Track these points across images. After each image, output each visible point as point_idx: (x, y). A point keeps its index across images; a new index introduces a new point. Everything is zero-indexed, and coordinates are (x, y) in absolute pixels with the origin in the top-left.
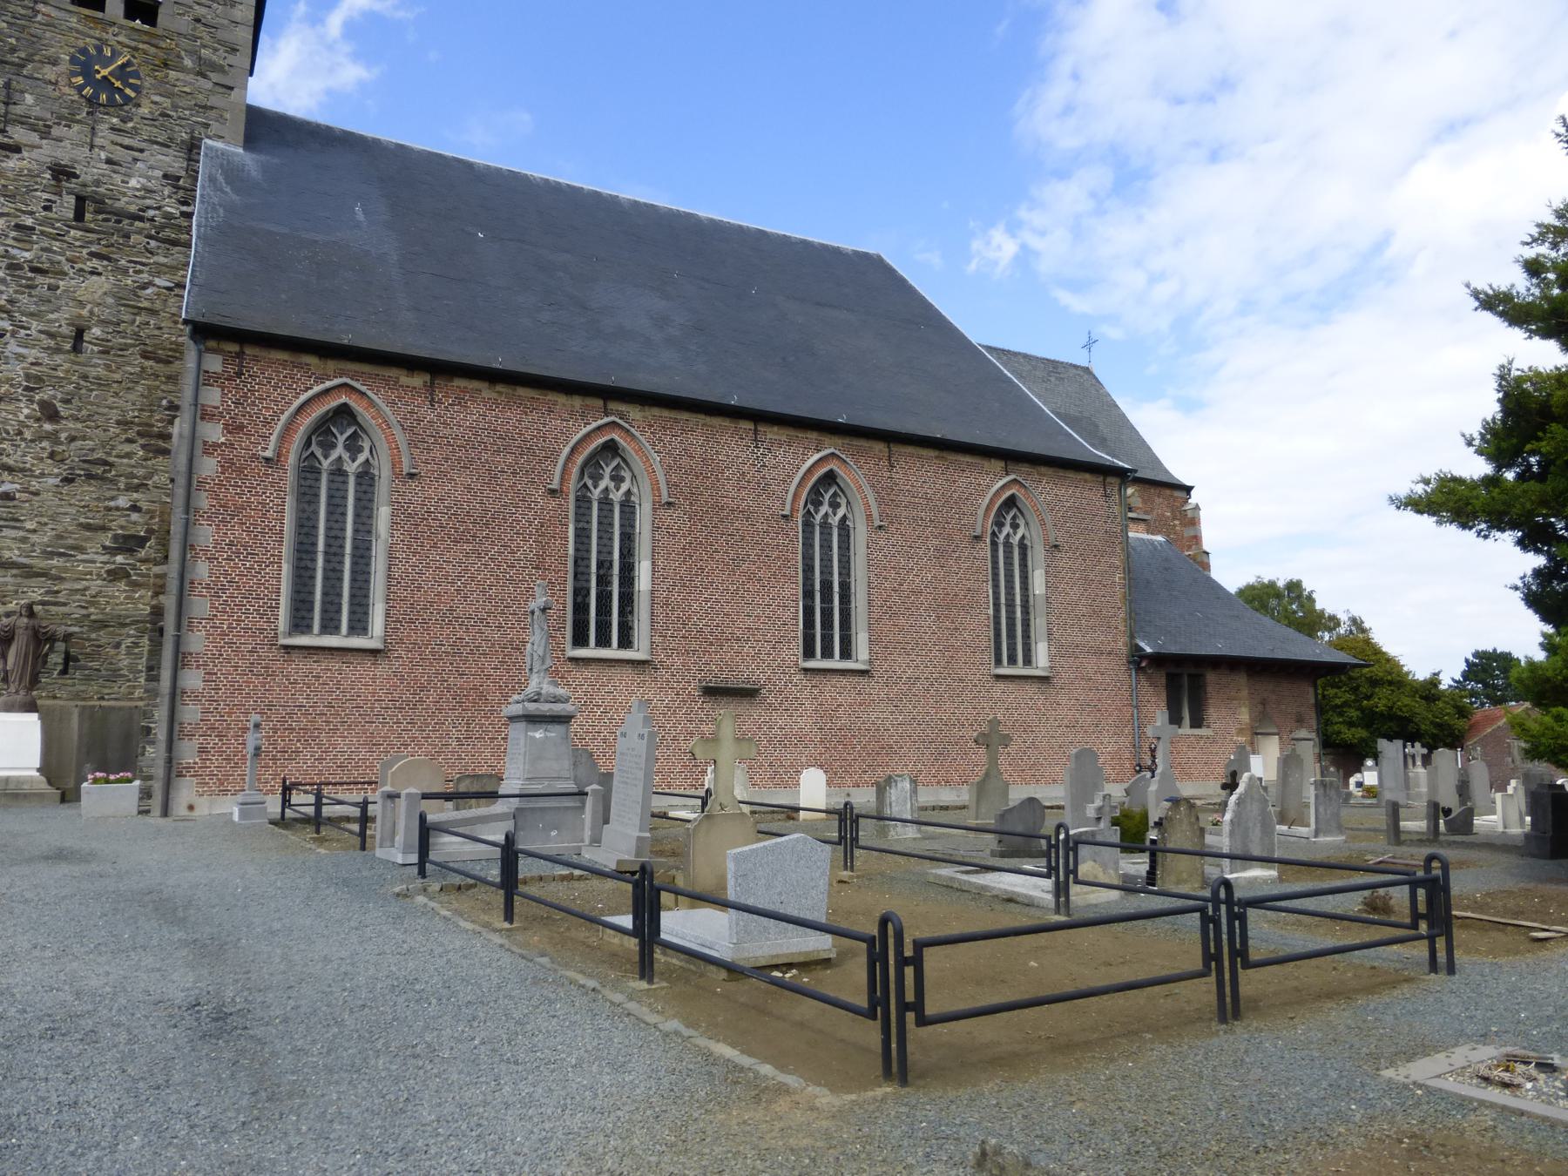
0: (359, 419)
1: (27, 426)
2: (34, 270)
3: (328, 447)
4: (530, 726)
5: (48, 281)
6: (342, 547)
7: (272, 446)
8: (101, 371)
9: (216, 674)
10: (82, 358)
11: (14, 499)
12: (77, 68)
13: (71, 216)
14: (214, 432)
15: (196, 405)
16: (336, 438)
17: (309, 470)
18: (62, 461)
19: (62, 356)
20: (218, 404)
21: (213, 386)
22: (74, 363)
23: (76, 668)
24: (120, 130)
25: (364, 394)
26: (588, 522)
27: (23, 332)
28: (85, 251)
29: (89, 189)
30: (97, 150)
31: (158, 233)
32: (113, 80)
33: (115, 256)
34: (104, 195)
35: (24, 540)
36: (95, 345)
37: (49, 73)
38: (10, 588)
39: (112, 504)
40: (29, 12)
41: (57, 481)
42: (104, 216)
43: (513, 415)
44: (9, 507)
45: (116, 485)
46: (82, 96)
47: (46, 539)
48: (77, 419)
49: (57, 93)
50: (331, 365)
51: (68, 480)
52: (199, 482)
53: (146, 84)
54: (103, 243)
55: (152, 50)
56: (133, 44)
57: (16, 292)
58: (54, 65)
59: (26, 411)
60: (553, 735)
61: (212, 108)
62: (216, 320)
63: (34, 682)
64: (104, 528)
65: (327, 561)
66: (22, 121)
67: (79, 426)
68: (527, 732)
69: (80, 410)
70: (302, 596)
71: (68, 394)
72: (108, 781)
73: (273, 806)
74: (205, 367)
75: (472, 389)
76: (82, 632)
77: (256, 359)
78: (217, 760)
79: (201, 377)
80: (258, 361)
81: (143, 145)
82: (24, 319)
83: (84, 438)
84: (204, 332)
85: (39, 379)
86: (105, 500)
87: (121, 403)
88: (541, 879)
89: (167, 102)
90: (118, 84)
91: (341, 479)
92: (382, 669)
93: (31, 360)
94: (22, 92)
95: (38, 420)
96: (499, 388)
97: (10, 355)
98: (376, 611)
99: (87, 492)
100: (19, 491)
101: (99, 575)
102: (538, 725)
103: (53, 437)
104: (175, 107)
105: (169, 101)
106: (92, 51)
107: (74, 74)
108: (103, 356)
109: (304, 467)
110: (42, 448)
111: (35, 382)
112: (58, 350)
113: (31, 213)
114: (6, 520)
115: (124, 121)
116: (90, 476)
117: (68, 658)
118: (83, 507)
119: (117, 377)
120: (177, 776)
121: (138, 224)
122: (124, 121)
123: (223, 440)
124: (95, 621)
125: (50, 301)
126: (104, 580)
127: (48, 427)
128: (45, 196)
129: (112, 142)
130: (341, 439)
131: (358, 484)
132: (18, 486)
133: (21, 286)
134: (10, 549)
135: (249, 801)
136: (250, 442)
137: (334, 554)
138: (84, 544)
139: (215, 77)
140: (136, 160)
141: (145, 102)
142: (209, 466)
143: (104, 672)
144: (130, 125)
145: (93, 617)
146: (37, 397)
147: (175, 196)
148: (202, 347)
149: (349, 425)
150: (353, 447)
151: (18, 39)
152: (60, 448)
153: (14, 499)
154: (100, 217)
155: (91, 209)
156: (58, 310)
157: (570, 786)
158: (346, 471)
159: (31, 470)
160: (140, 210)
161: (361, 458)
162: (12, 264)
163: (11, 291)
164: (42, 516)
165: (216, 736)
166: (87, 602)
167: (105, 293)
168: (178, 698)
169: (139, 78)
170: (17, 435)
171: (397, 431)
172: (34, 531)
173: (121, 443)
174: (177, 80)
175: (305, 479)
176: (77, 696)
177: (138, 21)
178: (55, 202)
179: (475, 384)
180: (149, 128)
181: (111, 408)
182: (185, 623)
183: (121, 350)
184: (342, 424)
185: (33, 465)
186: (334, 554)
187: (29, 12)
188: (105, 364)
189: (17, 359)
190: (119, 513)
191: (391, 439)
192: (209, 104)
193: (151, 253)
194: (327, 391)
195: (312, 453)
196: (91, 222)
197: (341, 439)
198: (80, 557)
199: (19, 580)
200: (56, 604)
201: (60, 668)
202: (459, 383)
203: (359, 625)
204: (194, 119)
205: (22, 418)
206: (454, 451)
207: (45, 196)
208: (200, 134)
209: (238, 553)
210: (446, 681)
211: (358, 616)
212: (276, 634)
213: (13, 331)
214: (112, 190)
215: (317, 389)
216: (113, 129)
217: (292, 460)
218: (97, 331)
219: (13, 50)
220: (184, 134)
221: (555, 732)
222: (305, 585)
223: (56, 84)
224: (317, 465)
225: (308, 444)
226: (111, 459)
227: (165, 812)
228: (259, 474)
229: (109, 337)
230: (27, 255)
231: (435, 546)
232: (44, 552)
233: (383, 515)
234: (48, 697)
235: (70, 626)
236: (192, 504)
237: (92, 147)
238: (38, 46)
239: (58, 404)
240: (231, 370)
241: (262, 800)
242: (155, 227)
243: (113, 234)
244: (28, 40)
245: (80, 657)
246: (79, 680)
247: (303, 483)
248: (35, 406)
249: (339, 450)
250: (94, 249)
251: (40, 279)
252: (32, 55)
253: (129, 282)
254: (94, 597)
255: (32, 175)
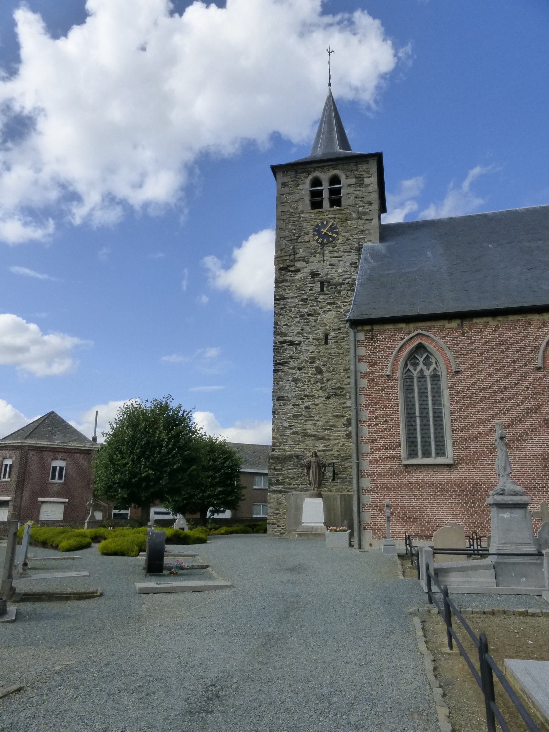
0: (428, 349)
1: (312, 378)
2: (309, 315)
3: (415, 365)
4: (501, 510)
5: (314, 318)
6: (428, 413)
7: (389, 370)
8: (336, 350)
9: (376, 480)
10: (328, 346)
11: (310, 408)
12: (315, 233)
13: (319, 290)
14: (364, 367)
15: (355, 357)
16: (419, 360)
17: (408, 379)
18: (325, 390)
19: (321, 347)
20: (365, 354)
21: (362, 346)
22: (326, 349)
23: (338, 478)
24: (332, 251)
25: (428, 336)
26: (419, 381)
27: (307, 340)
28: (325, 303)
29: (324, 278)
30: (325, 262)
31: (351, 288)
32: (328, 233)
33: (336, 302)
34: (330, 278)
35: (315, 425)
36: (333, 340)
37: (307, 238)
38: (311, 445)
39: (345, 405)
40: (298, 218)
41: (324, 399)
42: (331, 287)
43: (508, 332)
44: (308, 412)
45: (346, 397)
46: (318, 243)
47: (322, 423)
48: (329, 372)
49: (310, 245)
50: (412, 326)
51: (328, 398)
52: (360, 391)
53: (340, 230)
54: (331, 298)
55: (341, 216)
56: (334, 216)
57: (303, 325)
58: (308, 235)
59: (311, 372)
60: (516, 516)
61: (365, 230)
62: (360, 317)
63: (320, 484)
64: (343, 416)
65: (421, 421)
66: (300, 260)
67: (330, 374)
68: (498, 513)
69: (330, 368)
70: (411, 439)
71: (325, 362)
72: (336, 531)
73: (401, 546)
74: (357, 339)
75: (484, 322)
76: (338, 462)
77: (378, 331)
78: (380, 522)
79: (357, 344)
80: (379, 331)
81: (342, 254)
82: (307, 335)
83: (332, 379)
84: (355, 324)
85: (314, 358)
86: (342, 404)
87: (344, 362)
88: (505, 612)
89: (348, 234)
90: (330, 234)
91: (423, 379)
92: (454, 474)
93: (311, 351)
94: (298, 249)
95: (315, 374)
96: (499, 318)
97: (303, 350)
98: (448, 444)
99: (335, 402)
100: (311, 405)
101: (343, 437)
102: (504, 510)
103: (321, 381)
104: (351, 235)
105: (349, 233)
106: (320, 224)
107: (314, 236)
108: (336, 344)
109: (406, 376)
110: (318, 386)
111: (313, 359)
112: (320, 345)
113: (306, 293)
114: (308, 417)
115: (333, 247)
116: (336, 395)
117: (334, 474)
118: (334, 408)
119: (342, 351)
120: (364, 529)
121: (343, 286)
122: (333, 247)
123: (368, 370)
124: (343, 457)
125: (315, 326)
126: (345, 438)
127: (319, 377)
128: (310, 285)
129: (331, 257)
130: (421, 360)
131: (432, 381)
132: (311, 403)
133: (305, 323)
134: (310, 429)
135: (388, 544)
136: (380, 369)
137: (424, 417)
138: (336, 424)
139: (365, 217)
140: (339, 261)
141: (340, 237)
142: (363, 383)
143: (348, 479)
144: (336, 248)
145: (342, 455)
146: (314, 365)
147: (355, 271)
148: (356, 331)
149: (424, 353)
150: (427, 363)
151: (295, 230)
152: (324, 385)
153: (310, 408)
154: (329, 288)
155: (326, 286)
156: (318, 329)
157: (533, 549)
158: (425, 375)
159: (315, 396)
160: (343, 280)
161: (432, 368)
162: (301, 315)
163: (302, 325)
164: (320, 414)
165: (378, 510)
166: (339, 449)
167: (334, 318)
168: (361, 492)
169: (337, 229)
170: (309, 382)
171: (447, 351)
172: (318, 420)
173: (346, 379)
174: (351, 224)
175: (407, 382)
176: (339, 490)
177: (335, 207)
178: (313, 287)
179: (485, 319)
180: (343, 247)
181: (341, 365)
182: (360, 456)
183: (342, 340)
184: (421, 353)
185: (315, 393)
186: (424, 417)
187: (298, 218)
188: (337, 347)
189: (306, 352)
190: (348, 409)
191: (445, 356)
192: (364, 229)
193: (349, 297)
194: (411, 339)
195: (409, 369)
196: (326, 291)
197: (421, 360)
198: (335, 430)
199: (315, 441)
200: (328, 451)
201: (332, 478)
202: (476, 321)
203: (441, 452)
204: (359, 237)
205: (310, 375)
206: (478, 356)
207: (310, 285)
208: (362, 242)
209: (380, 421)
210: (490, 479)
211: (440, 447)
212: (400, 459)
213: (304, 341)
214: (332, 276)
215: (407, 338)
216: (331, 252)
217: (399, 374)
218: (333, 334)
219: (294, 234)
220: (356, 245)
221: (518, 513)
222: (412, 434)
223: (309, 241)
224: (412, 375)
225: (406, 365)
226: (343, 386)
227: (360, 547)
228: (385, 383)
229: (337, 335)
230: (306, 310)
231: (474, 407)
232: (322, 429)
233: (445, 394)
234: (328, 491)
235: (334, 459)
236: (358, 401)
237: (324, 261)
238: (302, 230)
239: (322, 367)
240: (369, 338)
241: (393, 544)
242: (349, 286)
243: (334, 293)
244: (298, 229)
245: (339, 473)
246: (339, 483)
247: (406, 384)
248: (314, 369)
249: (421, 366)
250: (328, 301)
251: (311, 318)
252: (301, 233)
253: (342, 311)
254: (342, 446)
255: (305, 279)
